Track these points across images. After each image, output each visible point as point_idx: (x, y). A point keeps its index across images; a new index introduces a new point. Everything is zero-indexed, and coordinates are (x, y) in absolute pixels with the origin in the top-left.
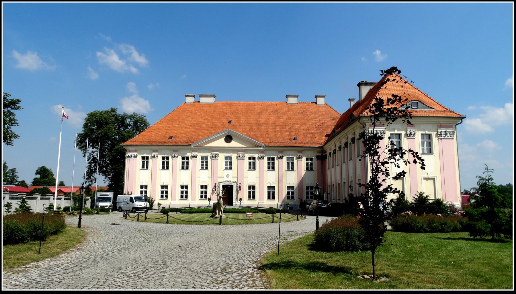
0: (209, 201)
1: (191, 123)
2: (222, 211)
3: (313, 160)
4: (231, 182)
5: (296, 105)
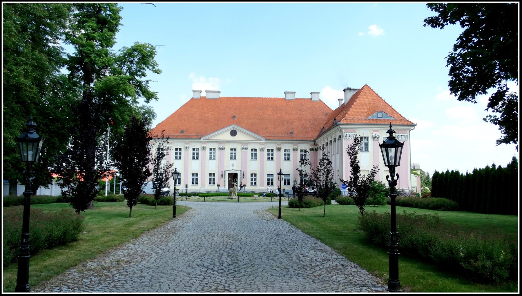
0: (218, 187)
1: (200, 117)
2: (236, 194)
3: (274, 151)
4: (236, 170)
5: (294, 101)
